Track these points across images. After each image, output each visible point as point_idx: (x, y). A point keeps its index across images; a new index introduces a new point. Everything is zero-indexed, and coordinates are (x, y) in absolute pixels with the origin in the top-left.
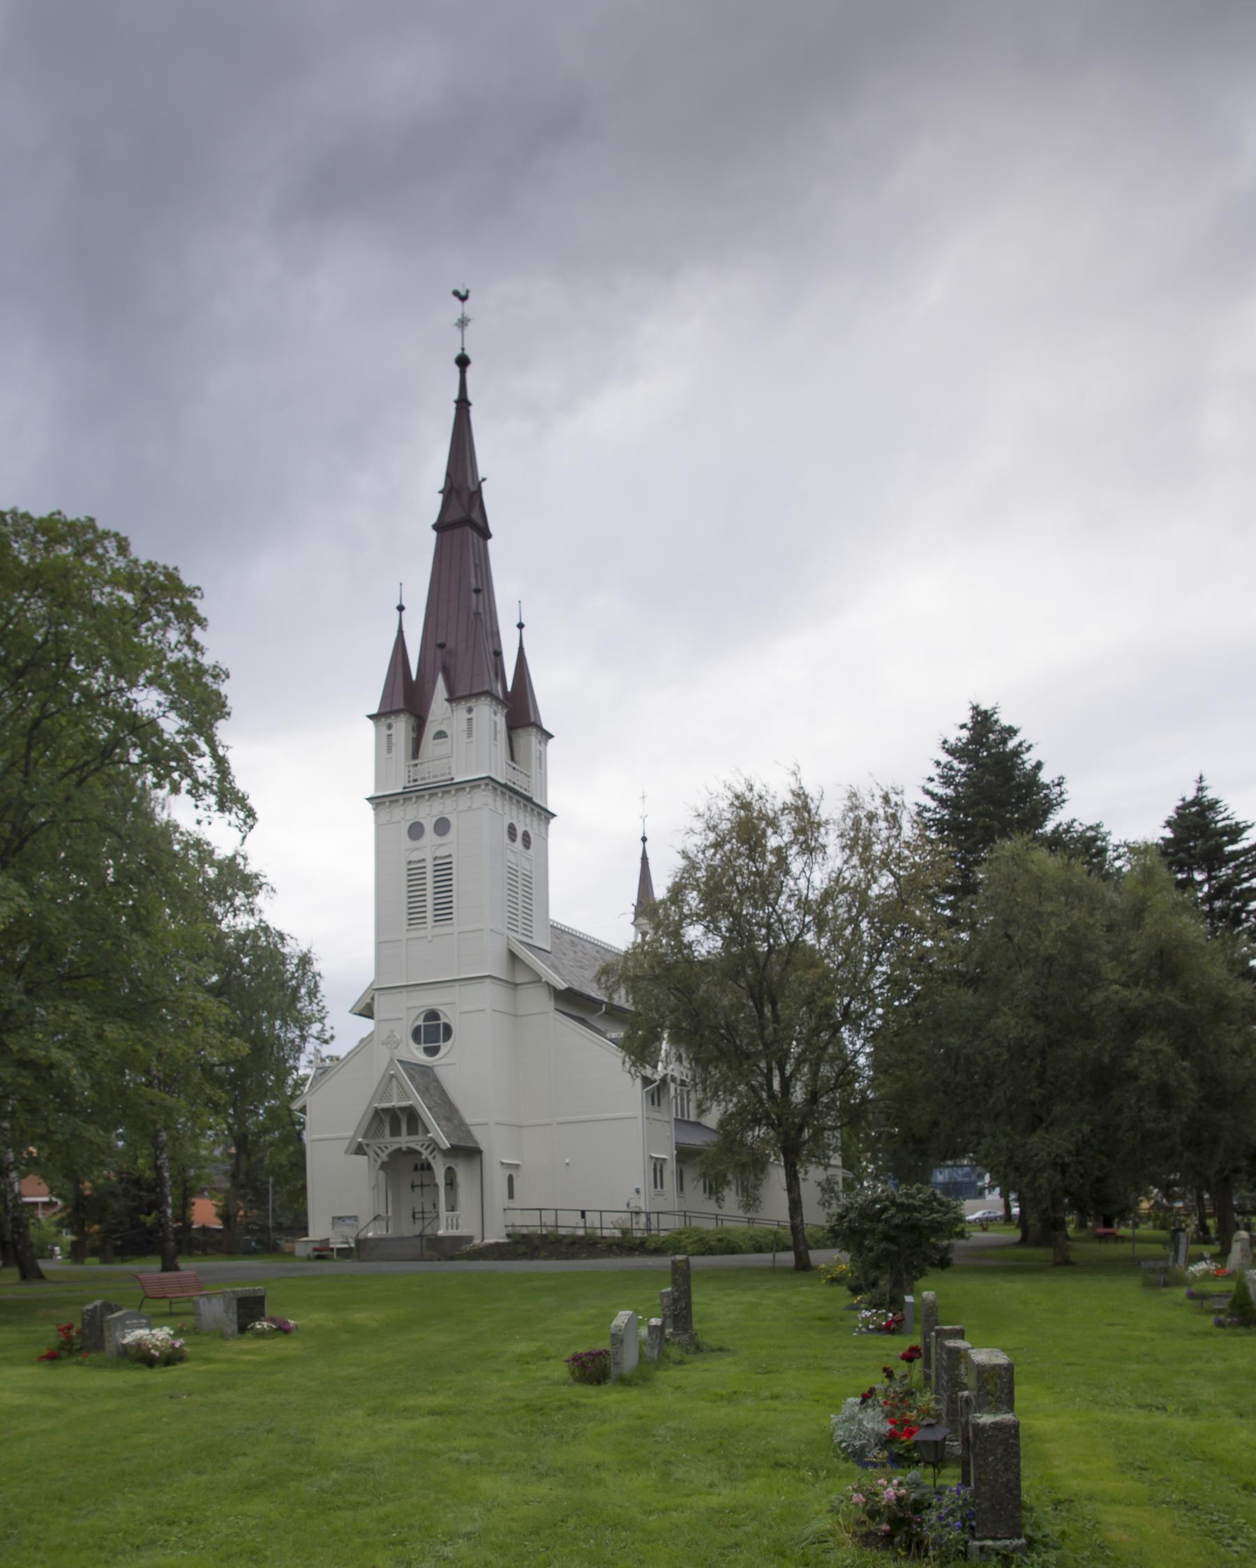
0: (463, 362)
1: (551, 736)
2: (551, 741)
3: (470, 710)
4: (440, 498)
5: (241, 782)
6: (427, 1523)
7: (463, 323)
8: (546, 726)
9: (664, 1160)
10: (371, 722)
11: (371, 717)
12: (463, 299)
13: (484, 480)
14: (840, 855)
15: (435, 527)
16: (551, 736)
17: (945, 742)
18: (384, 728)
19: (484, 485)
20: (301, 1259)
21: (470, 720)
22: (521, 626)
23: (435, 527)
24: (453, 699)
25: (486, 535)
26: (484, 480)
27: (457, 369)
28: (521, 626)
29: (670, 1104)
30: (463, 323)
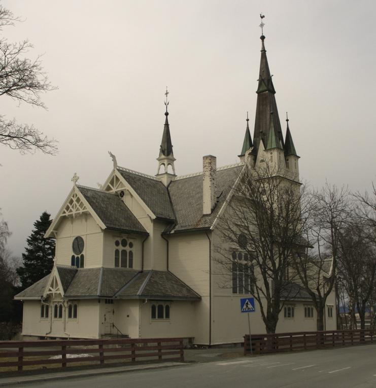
0: (263, 38)
1: (300, 157)
2: (299, 159)
3: (271, 153)
4: (258, 83)
5: (111, 158)
6: (154, 274)
7: (262, 25)
8: (298, 155)
9: (333, 306)
10: (239, 158)
11: (239, 156)
12: (262, 17)
13: (272, 76)
14: (32, 151)
15: (257, 92)
16: (300, 157)
17: (76, 174)
18: (269, 154)
19: (272, 77)
20: (226, 351)
21: (272, 156)
22: (287, 120)
23: (257, 92)
24: (266, 150)
25: (275, 92)
26: (272, 76)
27: (165, 116)
28: (287, 120)
29: (160, 179)
30: (262, 25)
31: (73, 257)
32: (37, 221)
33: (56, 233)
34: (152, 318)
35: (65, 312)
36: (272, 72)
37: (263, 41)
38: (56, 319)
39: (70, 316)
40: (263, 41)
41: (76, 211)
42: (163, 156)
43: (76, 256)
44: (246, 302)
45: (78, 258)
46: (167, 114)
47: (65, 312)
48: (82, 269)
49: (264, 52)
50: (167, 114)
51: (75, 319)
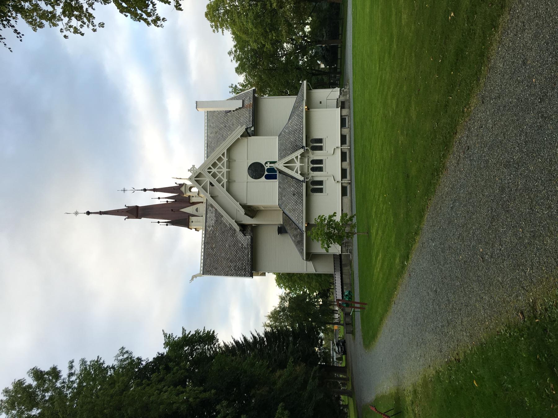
0: (88, 213)
25: (137, 207)
31: (268, 177)
35: (317, 155)
39: (320, 148)
40: (91, 213)
43: (266, 173)
46: (145, 190)
49: (101, 213)
50: (145, 190)
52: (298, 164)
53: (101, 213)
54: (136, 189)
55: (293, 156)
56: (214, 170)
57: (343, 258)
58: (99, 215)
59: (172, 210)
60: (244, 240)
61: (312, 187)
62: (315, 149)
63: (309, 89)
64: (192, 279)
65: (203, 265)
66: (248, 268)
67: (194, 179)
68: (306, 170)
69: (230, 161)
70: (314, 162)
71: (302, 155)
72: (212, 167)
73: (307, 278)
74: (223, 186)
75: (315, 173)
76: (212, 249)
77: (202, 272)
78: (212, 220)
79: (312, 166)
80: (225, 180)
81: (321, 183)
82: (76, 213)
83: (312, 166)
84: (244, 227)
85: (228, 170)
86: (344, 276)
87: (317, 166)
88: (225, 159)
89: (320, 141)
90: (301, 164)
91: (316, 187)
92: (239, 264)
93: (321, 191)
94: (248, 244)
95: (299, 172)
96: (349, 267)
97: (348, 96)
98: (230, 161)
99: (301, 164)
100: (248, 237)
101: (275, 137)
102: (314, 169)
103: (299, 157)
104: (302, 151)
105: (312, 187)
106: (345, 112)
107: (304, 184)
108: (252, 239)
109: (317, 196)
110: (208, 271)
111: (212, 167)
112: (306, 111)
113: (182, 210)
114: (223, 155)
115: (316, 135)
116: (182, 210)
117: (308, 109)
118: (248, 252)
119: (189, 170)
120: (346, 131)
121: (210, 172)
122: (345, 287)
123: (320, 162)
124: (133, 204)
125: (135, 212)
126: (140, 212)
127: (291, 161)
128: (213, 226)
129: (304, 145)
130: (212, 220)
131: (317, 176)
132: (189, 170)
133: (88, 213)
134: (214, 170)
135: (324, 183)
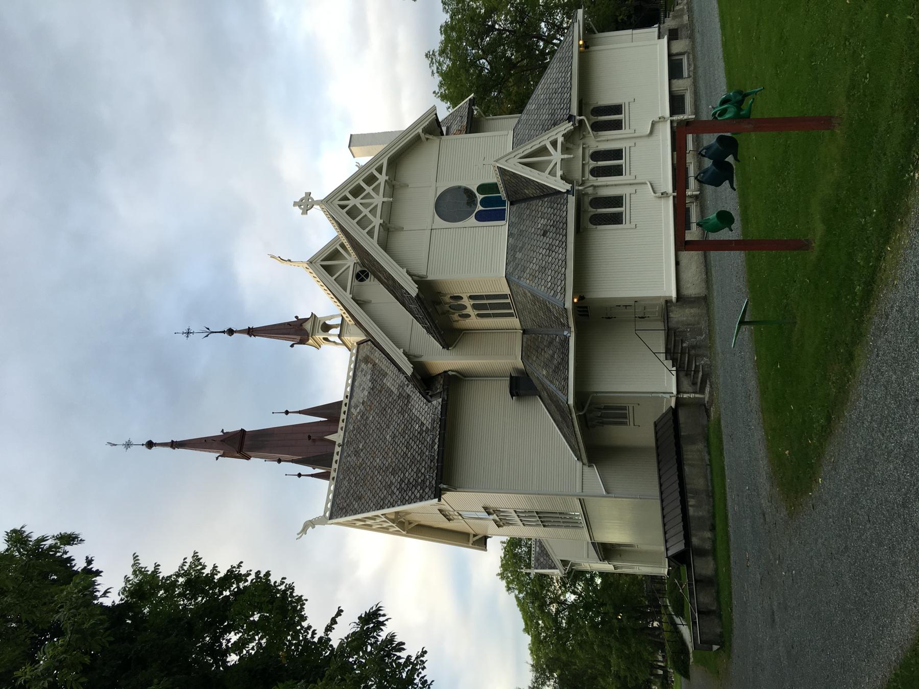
0: (150, 445)
13: (222, 431)
22: (287, 412)
25: (243, 431)
28: (287, 412)
31: (481, 217)
32: (404, 649)
33: (410, 523)
34: (620, 128)
35: (608, 141)
36: (214, 431)
37: (156, 445)
38: (626, 217)
39: (617, 125)
40: (156, 445)
41: (349, 199)
42: (310, 341)
43: (479, 208)
44: (545, 140)
45: (484, 202)
46: (231, 332)
47: (608, 141)
48: (501, 187)
49: (174, 445)
50: (231, 332)
51: (626, 110)
52: (557, 156)
53: (174, 445)
54: (212, 330)
55: (545, 140)
56: (353, 202)
57: (682, 418)
58: (169, 449)
59: (309, 437)
60: (425, 410)
61: (593, 211)
62: (598, 127)
63: (589, 32)
64: (304, 530)
65: (334, 497)
66: (431, 478)
67: (319, 263)
68: (577, 175)
69: (393, 187)
70: (597, 155)
71: (568, 137)
72: (350, 196)
73: (598, 646)
74: (371, 233)
75: (600, 179)
76: (357, 453)
77: (328, 514)
78: (364, 389)
79: (593, 164)
80: (377, 221)
81: (617, 201)
82: (128, 445)
83: (593, 164)
84: (425, 379)
85: (386, 199)
86: (687, 469)
87: (610, 163)
88: (382, 178)
89: (617, 109)
90: (566, 156)
91: (603, 212)
92: (410, 475)
93: (617, 219)
94: (433, 421)
95: (559, 173)
96: (700, 446)
97: (686, 18)
98: (393, 187)
99: (566, 156)
100: (437, 402)
101: (505, 132)
102: (598, 172)
103: (560, 140)
104: (568, 126)
105: (593, 211)
106: (680, 46)
107: (572, 200)
108: (445, 406)
109: (606, 234)
110: (342, 509)
111: (350, 196)
112: (580, 53)
113: (328, 437)
114: (380, 170)
115: (605, 98)
116: (328, 437)
117: (586, 46)
118: (433, 439)
119: (295, 204)
120: (680, 84)
121: (343, 207)
122: (692, 502)
123: (617, 154)
124: (232, 427)
125: (238, 444)
126: (247, 442)
127: (543, 151)
128: (363, 403)
129: (574, 111)
130: (364, 389)
131: (608, 186)
132: (295, 204)
133: (150, 445)
134: (353, 202)
135: (626, 202)
